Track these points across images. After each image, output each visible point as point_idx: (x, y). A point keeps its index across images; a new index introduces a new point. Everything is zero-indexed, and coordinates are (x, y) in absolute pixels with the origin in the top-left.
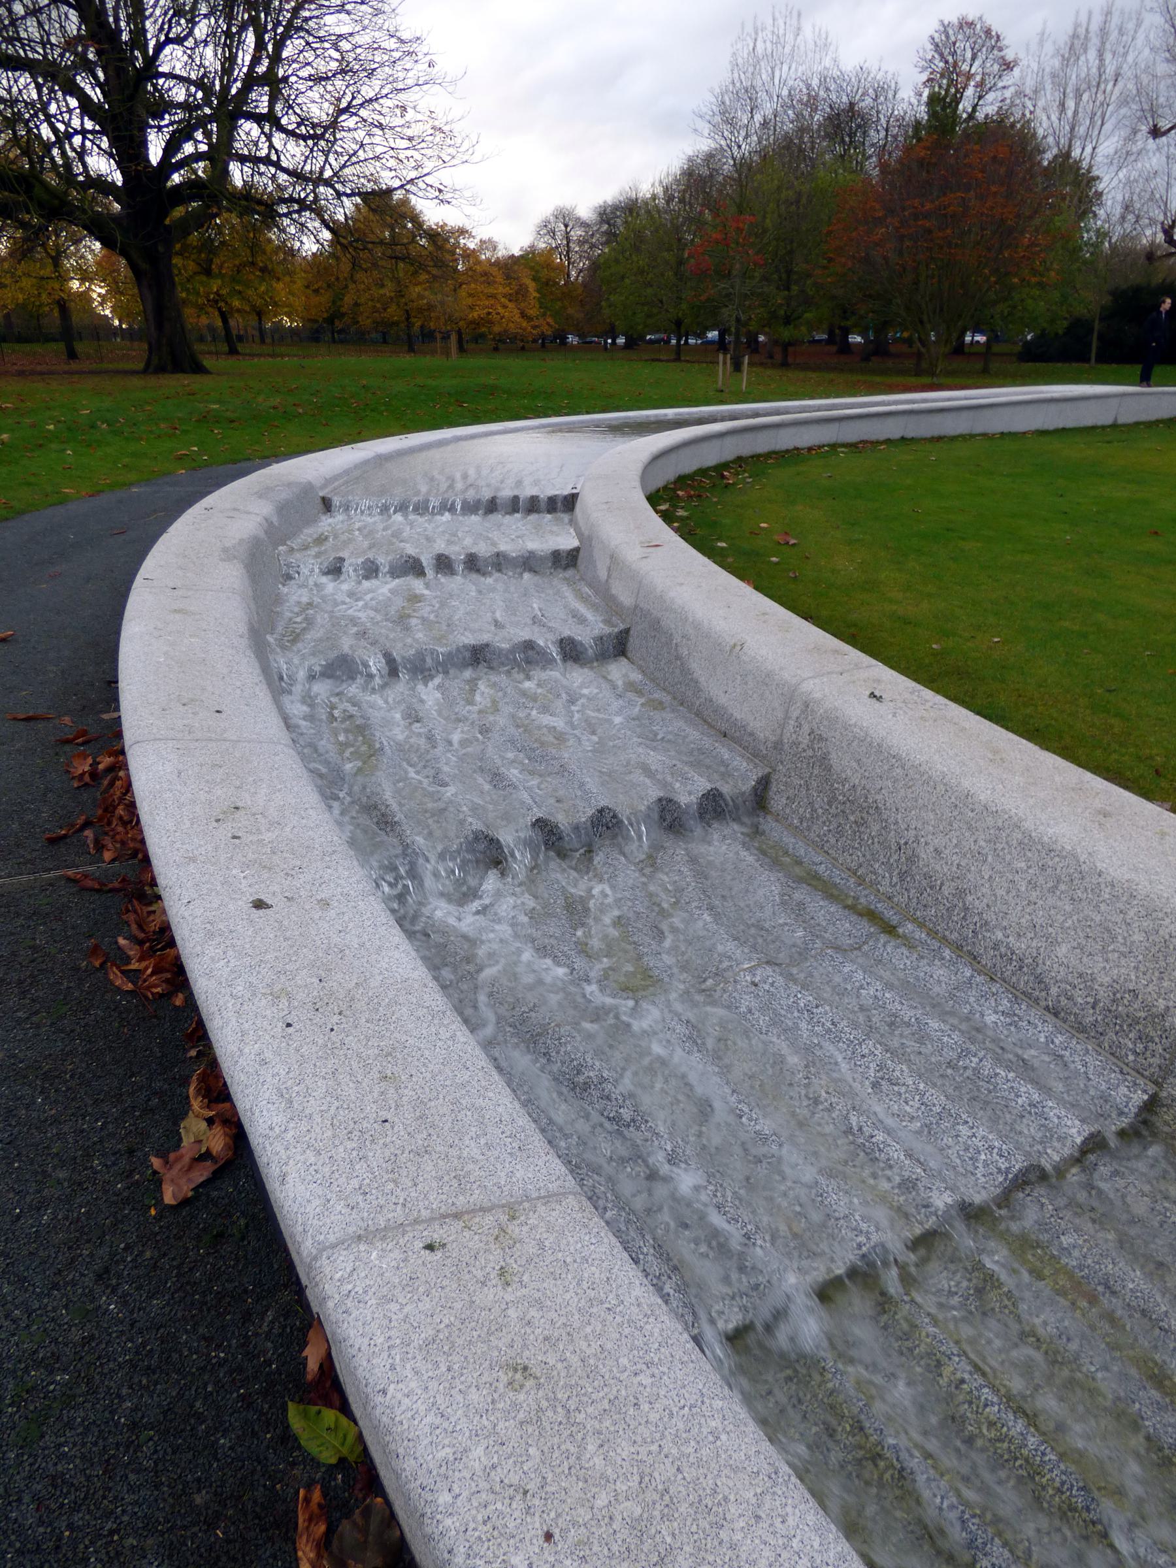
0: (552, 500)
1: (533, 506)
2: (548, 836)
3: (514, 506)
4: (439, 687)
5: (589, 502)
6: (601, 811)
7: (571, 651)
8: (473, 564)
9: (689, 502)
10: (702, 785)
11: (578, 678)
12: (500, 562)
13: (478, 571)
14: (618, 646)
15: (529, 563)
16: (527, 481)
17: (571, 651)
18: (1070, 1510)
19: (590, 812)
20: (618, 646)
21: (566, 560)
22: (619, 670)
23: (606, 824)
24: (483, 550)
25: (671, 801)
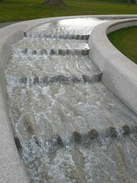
0: (83, 36)
1: (78, 37)
2: (77, 138)
3: (73, 37)
4: (54, 70)
5: (92, 38)
6: (93, 130)
7: (86, 79)
8: (61, 52)
9: (115, 36)
10: (123, 124)
11: (87, 85)
12: (68, 52)
13: (62, 54)
14: (99, 78)
15: (76, 52)
16: (77, 31)
17: (86, 79)
18: (133, 177)
19: (89, 130)
20: (99, 78)
21: (86, 53)
22: (98, 85)
23: (93, 135)
24: (64, 49)
25: (113, 128)
